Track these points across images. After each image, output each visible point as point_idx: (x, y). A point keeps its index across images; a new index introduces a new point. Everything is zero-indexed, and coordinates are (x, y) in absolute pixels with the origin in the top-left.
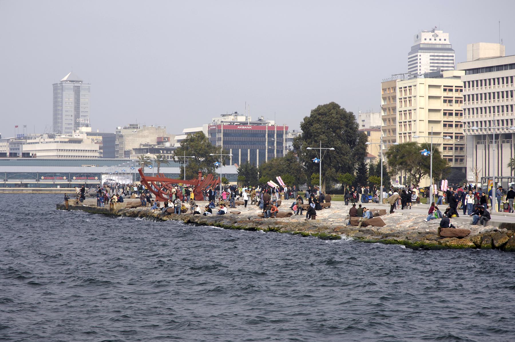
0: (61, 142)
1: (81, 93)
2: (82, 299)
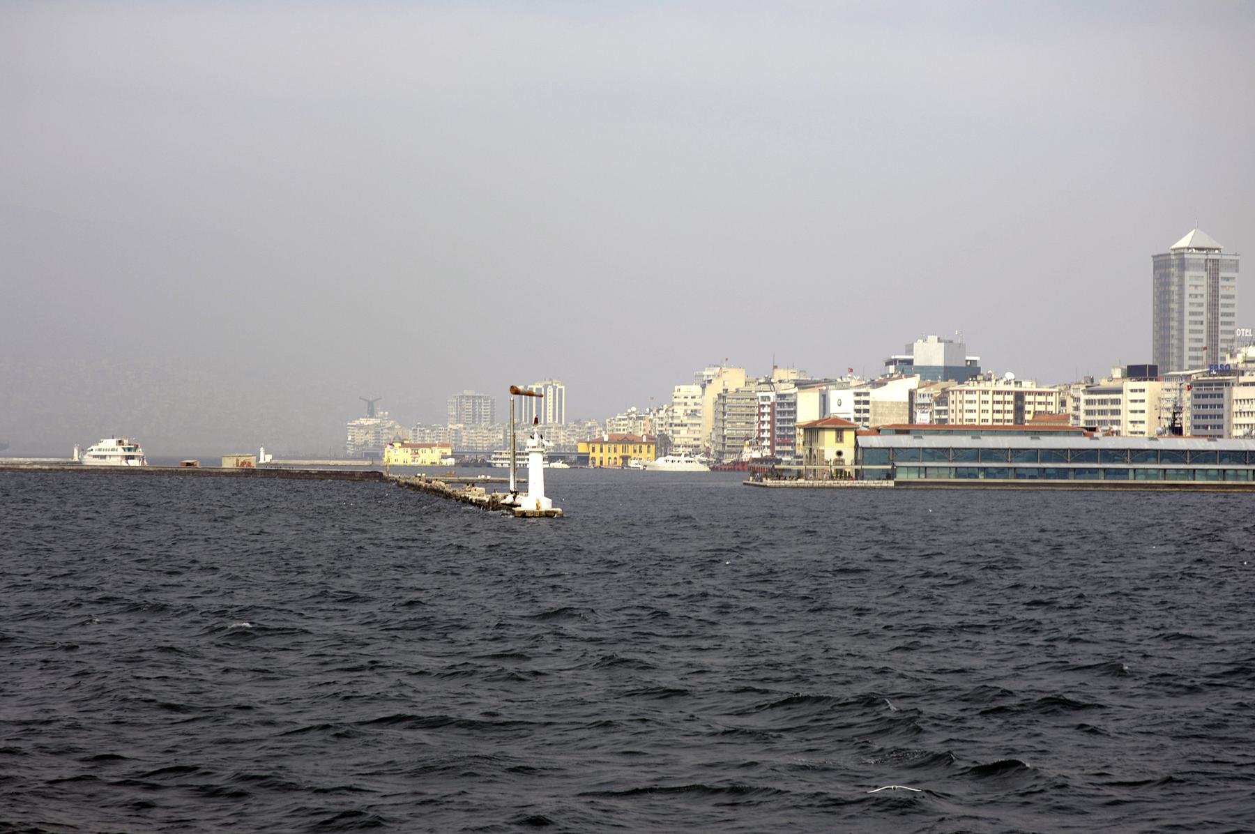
1: (1221, 274)
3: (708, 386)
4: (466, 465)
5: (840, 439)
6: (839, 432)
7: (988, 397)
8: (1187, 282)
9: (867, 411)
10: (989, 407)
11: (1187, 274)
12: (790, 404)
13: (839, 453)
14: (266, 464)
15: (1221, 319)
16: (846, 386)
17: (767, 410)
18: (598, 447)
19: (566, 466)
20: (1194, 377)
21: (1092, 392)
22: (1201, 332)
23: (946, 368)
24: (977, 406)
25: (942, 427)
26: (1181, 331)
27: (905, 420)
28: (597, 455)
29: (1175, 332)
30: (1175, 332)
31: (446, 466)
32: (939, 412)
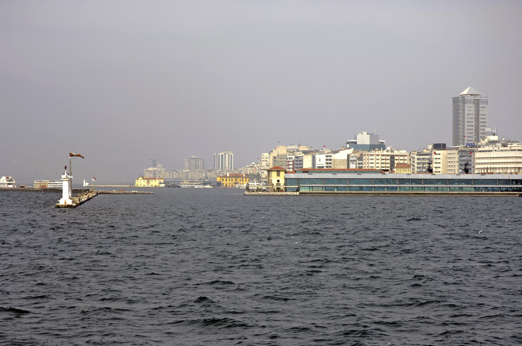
0: (518, 150)
1: (481, 106)
2: (24, 295)
3: (271, 153)
4: (169, 187)
5: (278, 175)
6: (278, 172)
7: (379, 157)
8: (466, 109)
9: (331, 163)
10: (379, 161)
11: (466, 105)
12: (300, 161)
13: (278, 181)
14: (86, 187)
15: (480, 124)
16: (323, 153)
17: (291, 163)
18: (225, 179)
19: (211, 187)
20: (460, 148)
21: (420, 155)
22: (472, 129)
23: (370, 145)
24: (375, 161)
25: (360, 170)
26: (464, 129)
27: (345, 167)
28: (224, 182)
29: (461, 130)
30: (461, 130)
31: (161, 187)
32: (359, 164)
